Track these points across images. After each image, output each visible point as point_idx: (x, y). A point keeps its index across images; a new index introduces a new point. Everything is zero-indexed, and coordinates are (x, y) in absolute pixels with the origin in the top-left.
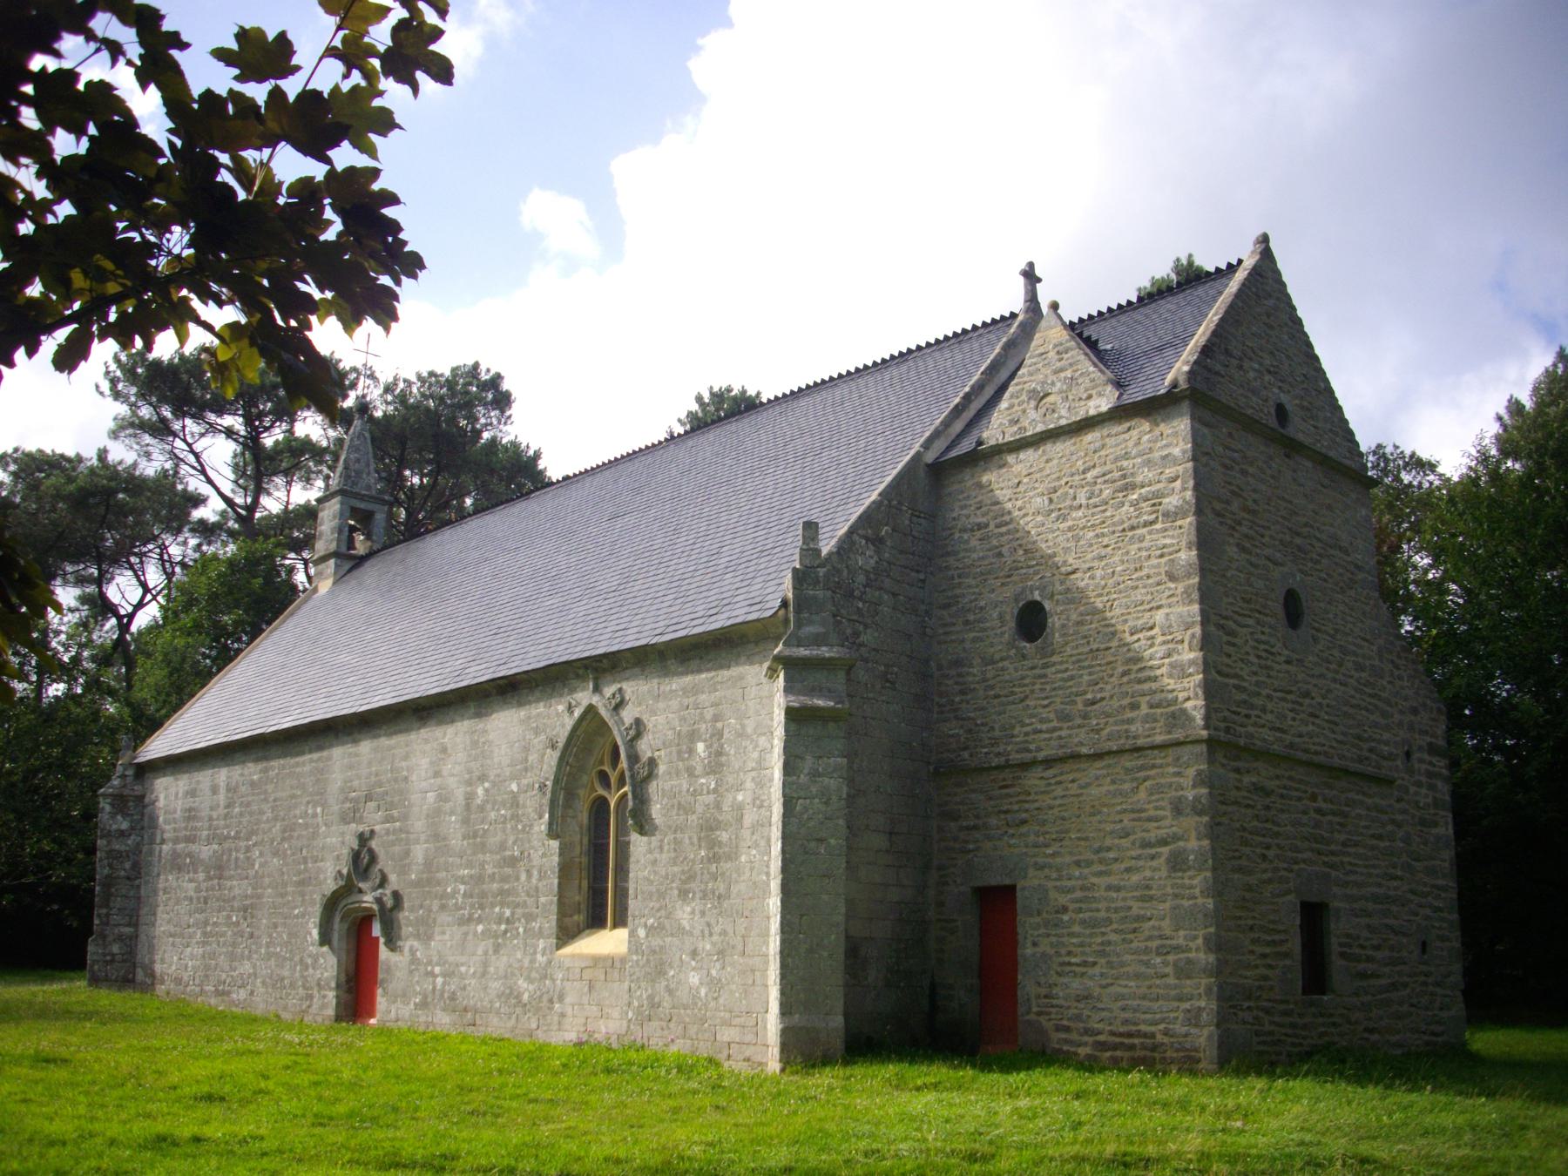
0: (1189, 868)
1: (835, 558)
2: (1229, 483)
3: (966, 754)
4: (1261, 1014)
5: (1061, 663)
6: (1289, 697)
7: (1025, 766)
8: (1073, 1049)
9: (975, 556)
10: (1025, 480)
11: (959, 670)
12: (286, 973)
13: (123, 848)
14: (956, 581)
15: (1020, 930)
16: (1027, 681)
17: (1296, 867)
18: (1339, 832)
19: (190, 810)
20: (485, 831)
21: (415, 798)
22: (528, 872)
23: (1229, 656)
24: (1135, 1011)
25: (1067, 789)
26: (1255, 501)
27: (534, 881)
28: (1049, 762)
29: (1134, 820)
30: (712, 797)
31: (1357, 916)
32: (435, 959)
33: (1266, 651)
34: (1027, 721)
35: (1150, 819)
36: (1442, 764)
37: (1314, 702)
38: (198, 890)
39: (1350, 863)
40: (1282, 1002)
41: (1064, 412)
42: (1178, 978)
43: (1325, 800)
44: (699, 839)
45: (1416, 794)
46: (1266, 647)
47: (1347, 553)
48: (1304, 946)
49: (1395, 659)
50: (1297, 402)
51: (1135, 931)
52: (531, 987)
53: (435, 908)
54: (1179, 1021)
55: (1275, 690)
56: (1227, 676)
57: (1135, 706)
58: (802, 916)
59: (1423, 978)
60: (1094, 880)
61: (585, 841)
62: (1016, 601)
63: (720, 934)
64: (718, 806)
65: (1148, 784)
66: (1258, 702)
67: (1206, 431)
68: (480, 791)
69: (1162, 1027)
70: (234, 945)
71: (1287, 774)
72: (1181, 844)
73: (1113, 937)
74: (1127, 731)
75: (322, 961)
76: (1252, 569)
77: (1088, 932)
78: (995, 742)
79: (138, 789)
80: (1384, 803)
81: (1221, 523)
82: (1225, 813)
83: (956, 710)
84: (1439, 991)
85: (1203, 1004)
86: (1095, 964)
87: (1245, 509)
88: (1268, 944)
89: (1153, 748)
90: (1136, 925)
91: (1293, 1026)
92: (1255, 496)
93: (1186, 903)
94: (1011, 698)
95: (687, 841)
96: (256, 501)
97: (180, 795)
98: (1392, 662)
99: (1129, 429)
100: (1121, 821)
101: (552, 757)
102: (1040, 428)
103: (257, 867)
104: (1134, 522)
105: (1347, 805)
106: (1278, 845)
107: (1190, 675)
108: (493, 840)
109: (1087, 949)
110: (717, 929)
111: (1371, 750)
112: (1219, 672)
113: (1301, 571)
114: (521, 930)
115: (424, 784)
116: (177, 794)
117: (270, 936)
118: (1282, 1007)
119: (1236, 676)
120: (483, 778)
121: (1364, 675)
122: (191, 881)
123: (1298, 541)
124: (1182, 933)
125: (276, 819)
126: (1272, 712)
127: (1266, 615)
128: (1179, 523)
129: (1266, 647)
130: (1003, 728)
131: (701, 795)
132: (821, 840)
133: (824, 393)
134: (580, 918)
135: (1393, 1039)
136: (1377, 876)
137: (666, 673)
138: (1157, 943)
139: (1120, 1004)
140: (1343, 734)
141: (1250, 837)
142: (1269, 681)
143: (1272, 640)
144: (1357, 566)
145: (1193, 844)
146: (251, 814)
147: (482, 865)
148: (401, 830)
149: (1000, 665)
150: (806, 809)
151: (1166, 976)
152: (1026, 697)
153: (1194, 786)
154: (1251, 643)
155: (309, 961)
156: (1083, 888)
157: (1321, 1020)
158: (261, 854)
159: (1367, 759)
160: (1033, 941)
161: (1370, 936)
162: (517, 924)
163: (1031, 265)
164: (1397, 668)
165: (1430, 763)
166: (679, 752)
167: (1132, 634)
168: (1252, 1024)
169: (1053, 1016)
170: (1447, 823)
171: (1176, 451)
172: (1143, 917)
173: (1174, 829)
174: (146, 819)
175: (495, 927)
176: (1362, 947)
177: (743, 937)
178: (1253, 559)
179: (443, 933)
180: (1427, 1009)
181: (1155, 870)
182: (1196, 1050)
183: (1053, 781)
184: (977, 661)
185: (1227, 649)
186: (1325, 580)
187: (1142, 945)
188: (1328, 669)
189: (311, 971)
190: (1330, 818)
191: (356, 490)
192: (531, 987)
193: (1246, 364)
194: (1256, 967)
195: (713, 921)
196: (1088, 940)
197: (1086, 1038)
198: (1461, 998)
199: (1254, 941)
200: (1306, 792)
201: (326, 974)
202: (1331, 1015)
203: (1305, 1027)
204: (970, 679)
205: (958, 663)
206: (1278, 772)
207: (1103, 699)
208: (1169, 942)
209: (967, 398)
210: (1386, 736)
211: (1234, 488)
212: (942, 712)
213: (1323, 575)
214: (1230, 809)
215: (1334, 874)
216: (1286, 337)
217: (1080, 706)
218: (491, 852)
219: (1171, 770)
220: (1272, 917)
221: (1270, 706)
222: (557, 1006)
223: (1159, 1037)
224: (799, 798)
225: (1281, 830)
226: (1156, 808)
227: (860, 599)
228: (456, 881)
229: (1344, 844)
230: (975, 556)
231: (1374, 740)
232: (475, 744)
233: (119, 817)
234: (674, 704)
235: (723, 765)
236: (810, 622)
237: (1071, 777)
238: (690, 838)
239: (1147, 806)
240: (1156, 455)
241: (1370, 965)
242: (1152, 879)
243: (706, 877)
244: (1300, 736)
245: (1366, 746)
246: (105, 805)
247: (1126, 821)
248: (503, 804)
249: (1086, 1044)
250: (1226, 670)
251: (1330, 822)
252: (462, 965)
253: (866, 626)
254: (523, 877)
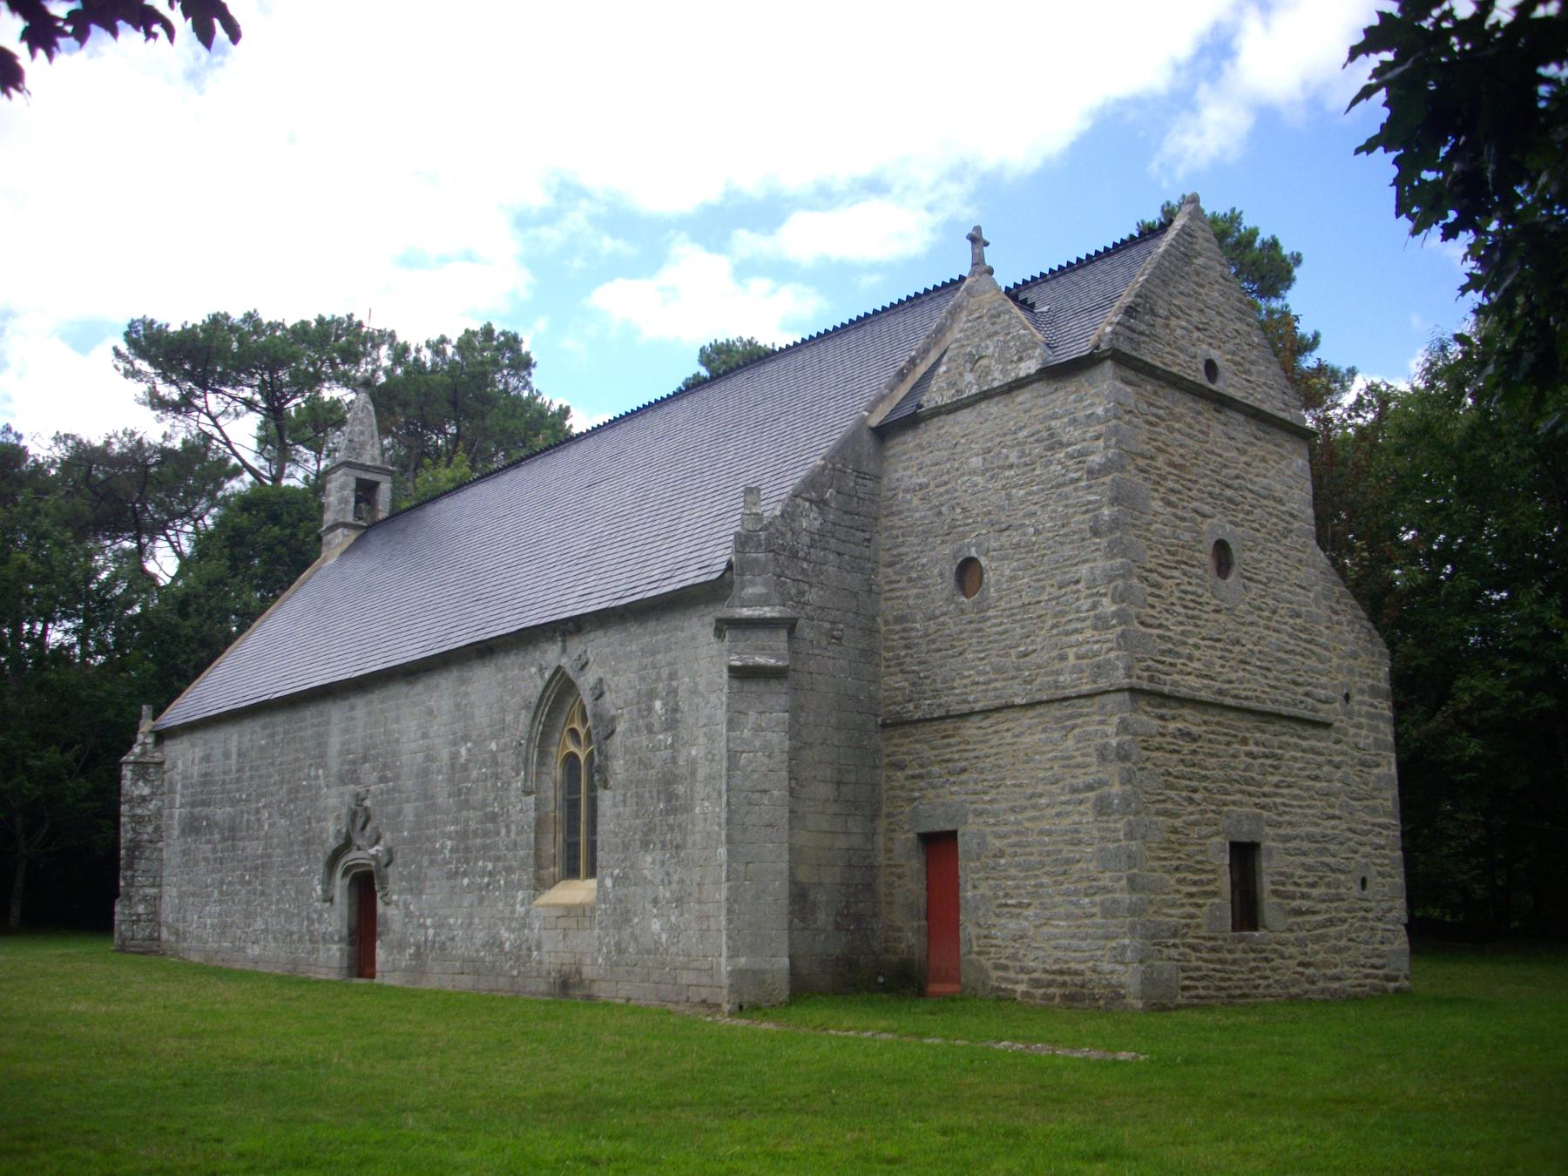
0: (1114, 812)
1: (779, 522)
2: (1154, 440)
3: (911, 706)
4: (1187, 950)
5: (996, 617)
6: (1218, 645)
7: (963, 716)
8: (1010, 987)
9: (917, 515)
10: (963, 441)
11: (905, 625)
12: (295, 929)
13: (146, 812)
14: (901, 539)
15: (961, 873)
16: (965, 635)
17: (1225, 809)
18: (1272, 774)
19: (206, 775)
20: (469, 789)
21: (405, 758)
22: (507, 826)
23: (1153, 607)
24: (1066, 949)
25: (1003, 738)
26: (1182, 456)
27: (513, 835)
28: (986, 712)
29: (1063, 767)
30: (669, 751)
31: (1291, 855)
32: (426, 911)
33: (1193, 601)
34: (966, 673)
35: (1078, 766)
36: (1384, 705)
37: (1245, 650)
38: (214, 851)
39: (1284, 805)
40: (1210, 939)
41: (997, 375)
42: (1104, 917)
43: (1257, 744)
44: (659, 792)
45: (1356, 735)
46: (1194, 597)
47: (1280, 501)
48: (1233, 884)
49: (1334, 605)
50: (1229, 357)
51: (1065, 873)
52: (512, 937)
53: (425, 863)
54: (1106, 958)
55: (1203, 639)
56: (1151, 626)
57: (1063, 658)
58: (747, 863)
59: (1362, 913)
60: (1028, 825)
61: (559, 795)
62: (955, 558)
63: (678, 883)
64: (674, 760)
65: (1076, 731)
66: (1185, 651)
67: (1129, 389)
68: (463, 751)
69: (1090, 964)
70: (248, 903)
71: (1216, 719)
72: (1106, 789)
73: (1045, 880)
74: (1056, 682)
75: (326, 916)
76: (1178, 522)
77: (1022, 875)
78: (937, 693)
79: (158, 756)
80: (1319, 744)
81: (1145, 479)
82: (1148, 759)
83: (901, 664)
84: (1380, 925)
85: (1127, 941)
86: (1029, 905)
87: (1172, 464)
88: (1195, 883)
89: (1079, 697)
90: (1065, 867)
91: (1221, 961)
92: (1181, 451)
93: (1111, 846)
94: (951, 652)
95: (647, 795)
96: (281, 470)
97: (197, 761)
98: (1331, 607)
99: (1056, 389)
100: (1052, 768)
101: (525, 718)
102: (974, 390)
103: (266, 827)
104: (1061, 480)
105: (1280, 748)
106: (1205, 788)
107: (1114, 626)
108: (477, 798)
109: (1022, 891)
110: (676, 878)
111: (1307, 694)
112: (1142, 623)
113: (1231, 522)
114: (502, 882)
115: (413, 745)
116: (193, 760)
117: (279, 893)
118: (1210, 944)
119: (1160, 626)
120: (466, 738)
121: (1298, 621)
122: (208, 842)
123: (1229, 493)
124: (1107, 874)
125: (282, 782)
126: (1199, 660)
127: (1193, 566)
128: (1102, 480)
129: (1194, 597)
130: (944, 681)
131: (659, 750)
132: (765, 791)
133: (788, 358)
134: (556, 870)
135: (1330, 972)
136: (1313, 815)
137: (634, 629)
138: (1086, 884)
139: (1052, 943)
140: (1276, 678)
141: (1174, 780)
142: (1196, 630)
143: (1200, 591)
144: (1292, 515)
145: (1116, 789)
146: (260, 777)
147: (466, 821)
148: (394, 790)
149: (942, 619)
150: (750, 762)
151: (1093, 915)
152: (965, 650)
153: (1117, 734)
154: (1177, 594)
155: (315, 916)
156: (1017, 833)
157: (1252, 955)
158: (270, 816)
159: (1301, 702)
160: (973, 888)
161: (1305, 873)
162: (498, 877)
163: (978, 229)
164: (1336, 613)
165: (1372, 705)
166: (639, 710)
167: (1060, 588)
168: (1178, 960)
169: (992, 955)
170: (1389, 763)
171: (1100, 411)
172: (1073, 858)
173: (1100, 775)
174: (166, 784)
175: (479, 880)
176: (1296, 884)
177: (699, 885)
178: (1179, 513)
179: (433, 886)
180: (1367, 943)
181: (1083, 814)
182: (1122, 986)
183: (990, 730)
184: (919, 616)
185: (1151, 600)
186: (1258, 530)
187: (1072, 887)
188: (1259, 617)
189: (316, 925)
190: (1262, 760)
191: (360, 461)
192: (512, 937)
193: (1173, 322)
194: (1183, 905)
195: (671, 870)
196: (1022, 883)
197: (1022, 976)
198: (1404, 932)
199: (1179, 881)
200: (1236, 736)
201: (330, 929)
202: (1263, 951)
203: (1234, 962)
204: (914, 634)
205: (901, 619)
206: (1206, 717)
207: (1034, 651)
208: (1095, 883)
209: (913, 362)
210: (1323, 680)
211: (1159, 444)
212: (889, 667)
213: (1256, 525)
214: (1154, 754)
215: (1265, 814)
216: (1216, 294)
217: (1013, 658)
218: (474, 809)
219: (1097, 718)
220: (1199, 858)
221: (1197, 654)
222: (535, 953)
223: (1088, 973)
224: (743, 752)
225: (1209, 773)
226: (1083, 755)
227: (805, 559)
228: (444, 837)
229: (1277, 786)
230: (917, 515)
231: (1309, 684)
232: (458, 705)
233: (140, 783)
234: (635, 664)
235: (678, 722)
236: (753, 583)
237: (1006, 726)
238: (650, 792)
239: (1075, 753)
240: (1081, 415)
241: (1305, 902)
242: (1080, 823)
243: (665, 828)
244: (1230, 682)
245: (1301, 690)
246: (127, 772)
247: (1056, 768)
248: (484, 764)
249: (1022, 982)
250: (1149, 620)
251: (1262, 764)
252: (451, 916)
253: (811, 585)
254: (503, 831)
